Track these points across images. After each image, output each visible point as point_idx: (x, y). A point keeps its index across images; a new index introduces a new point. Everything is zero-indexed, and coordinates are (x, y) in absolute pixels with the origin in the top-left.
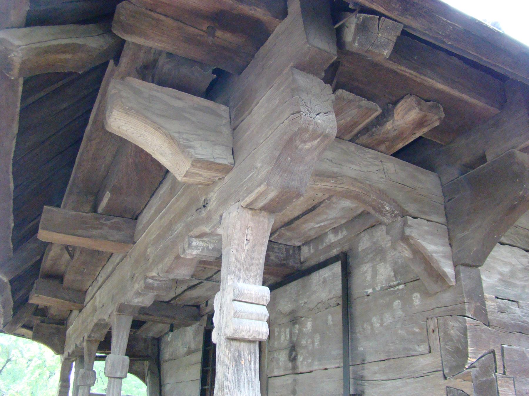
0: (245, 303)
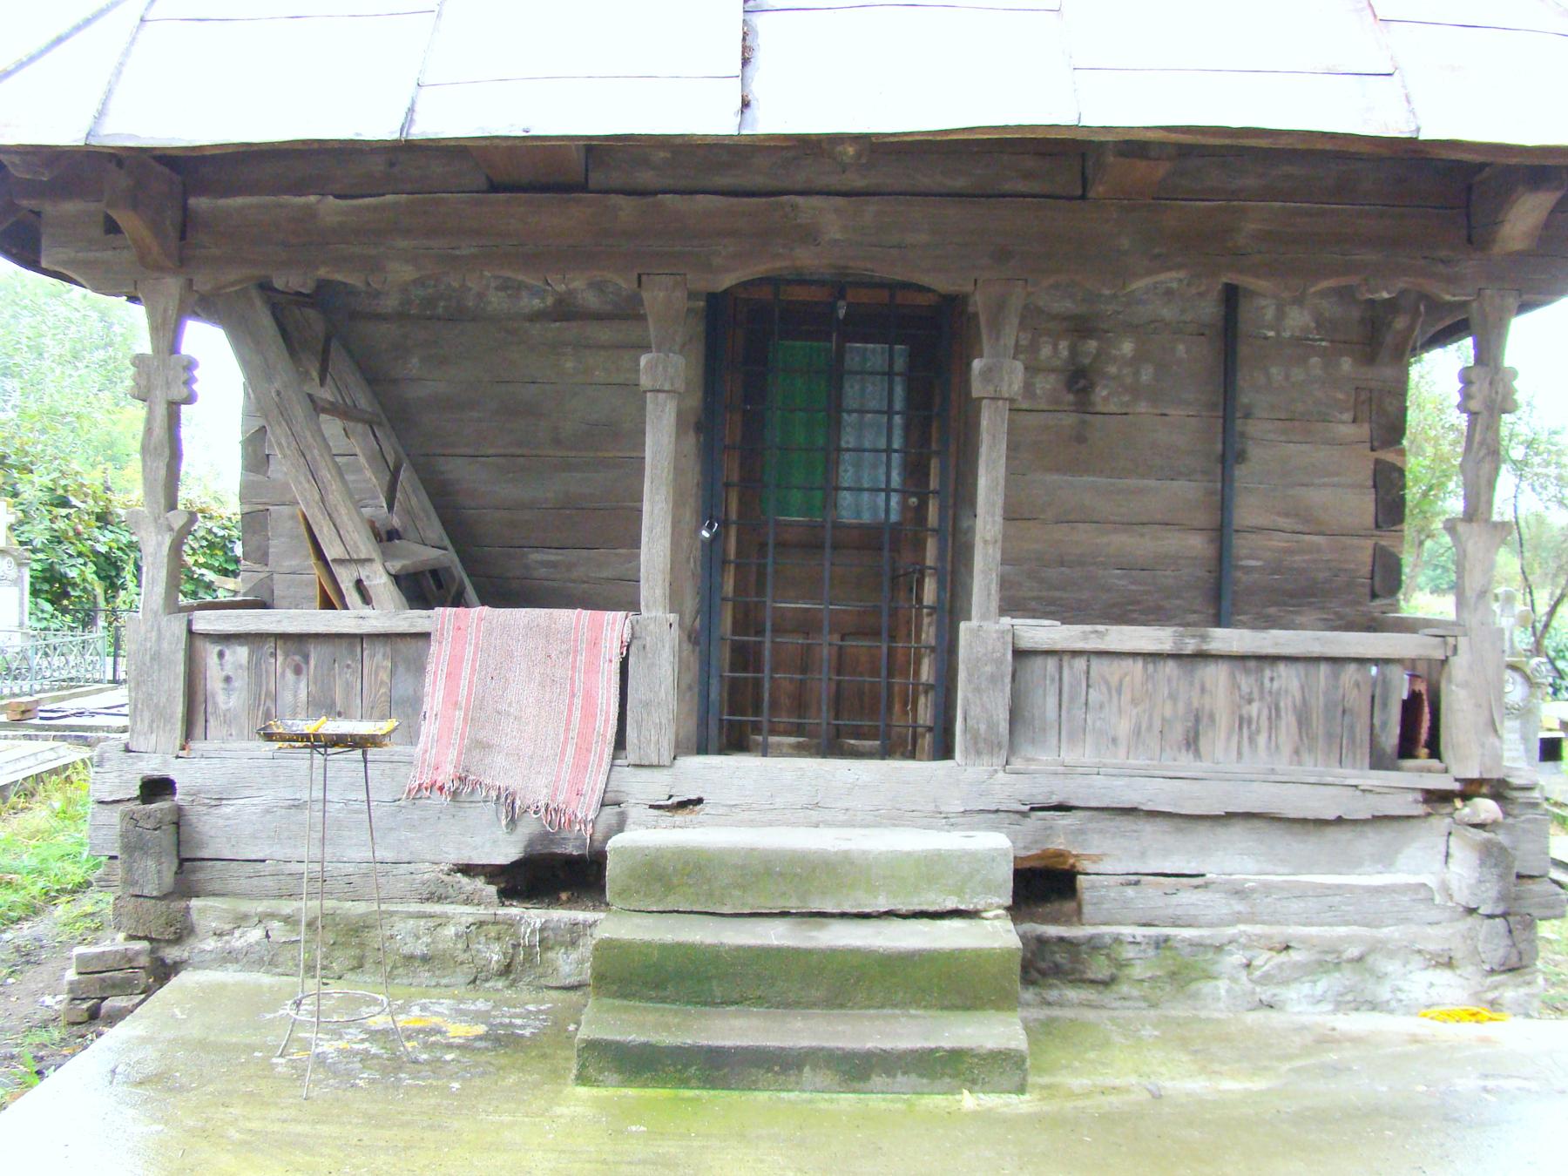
0: (925, 921)
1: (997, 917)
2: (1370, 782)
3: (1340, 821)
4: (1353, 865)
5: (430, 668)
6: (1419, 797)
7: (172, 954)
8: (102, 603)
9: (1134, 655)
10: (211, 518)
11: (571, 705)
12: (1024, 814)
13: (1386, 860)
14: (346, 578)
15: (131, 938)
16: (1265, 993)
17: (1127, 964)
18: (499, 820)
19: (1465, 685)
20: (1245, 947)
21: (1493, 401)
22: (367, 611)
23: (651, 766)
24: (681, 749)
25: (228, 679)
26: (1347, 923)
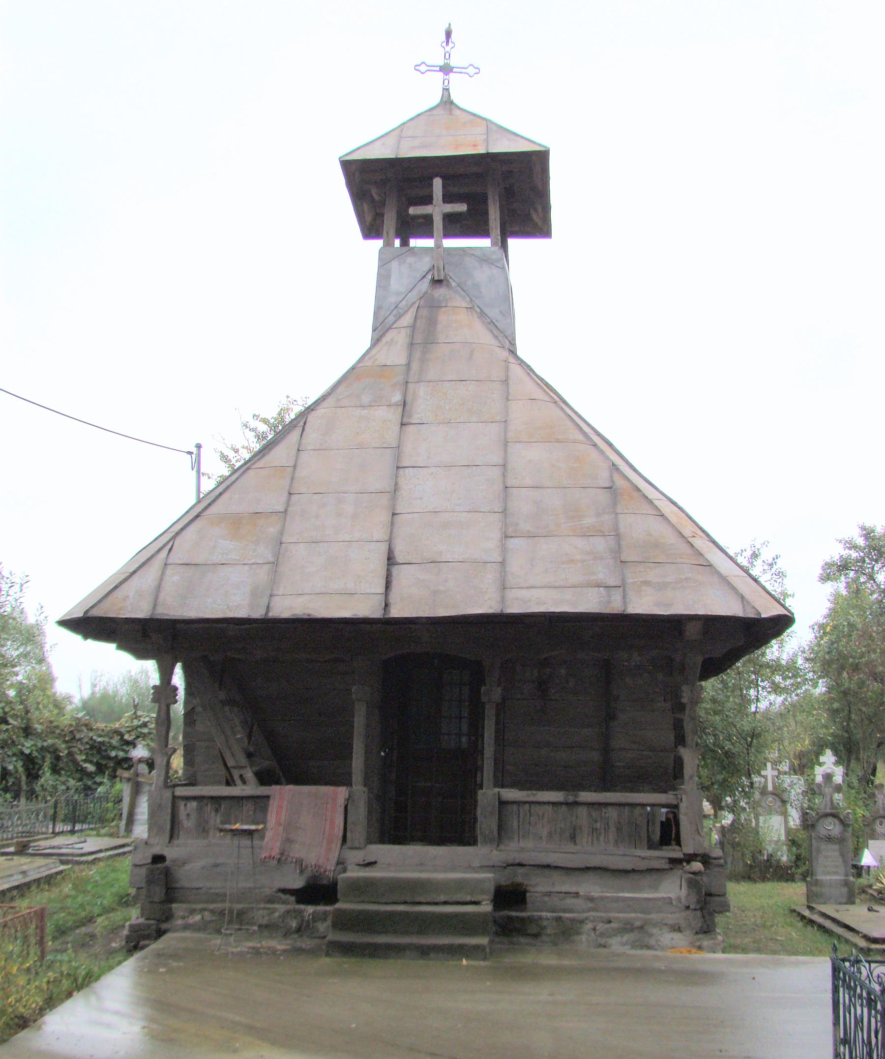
1: (486, 904)
2: (646, 854)
3: (634, 871)
4: (641, 889)
5: (270, 810)
6: (667, 861)
7: (164, 926)
8: (25, 787)
9: (549, 803)
10: (91, 730)
11: (325, 824)
12: (505, 867)
13: (655, 887)
14: (236, 774)
15: (147, 919)
16: (602, 941)
17: (545, 927)
18: (296, 870)
19: (686, 815)
20: (592, 921)
21: (693, 699)
22: (244, 787)
23: (356, 848)
24: (370, 841)
25: (188, 815)
26: (635, 912)
